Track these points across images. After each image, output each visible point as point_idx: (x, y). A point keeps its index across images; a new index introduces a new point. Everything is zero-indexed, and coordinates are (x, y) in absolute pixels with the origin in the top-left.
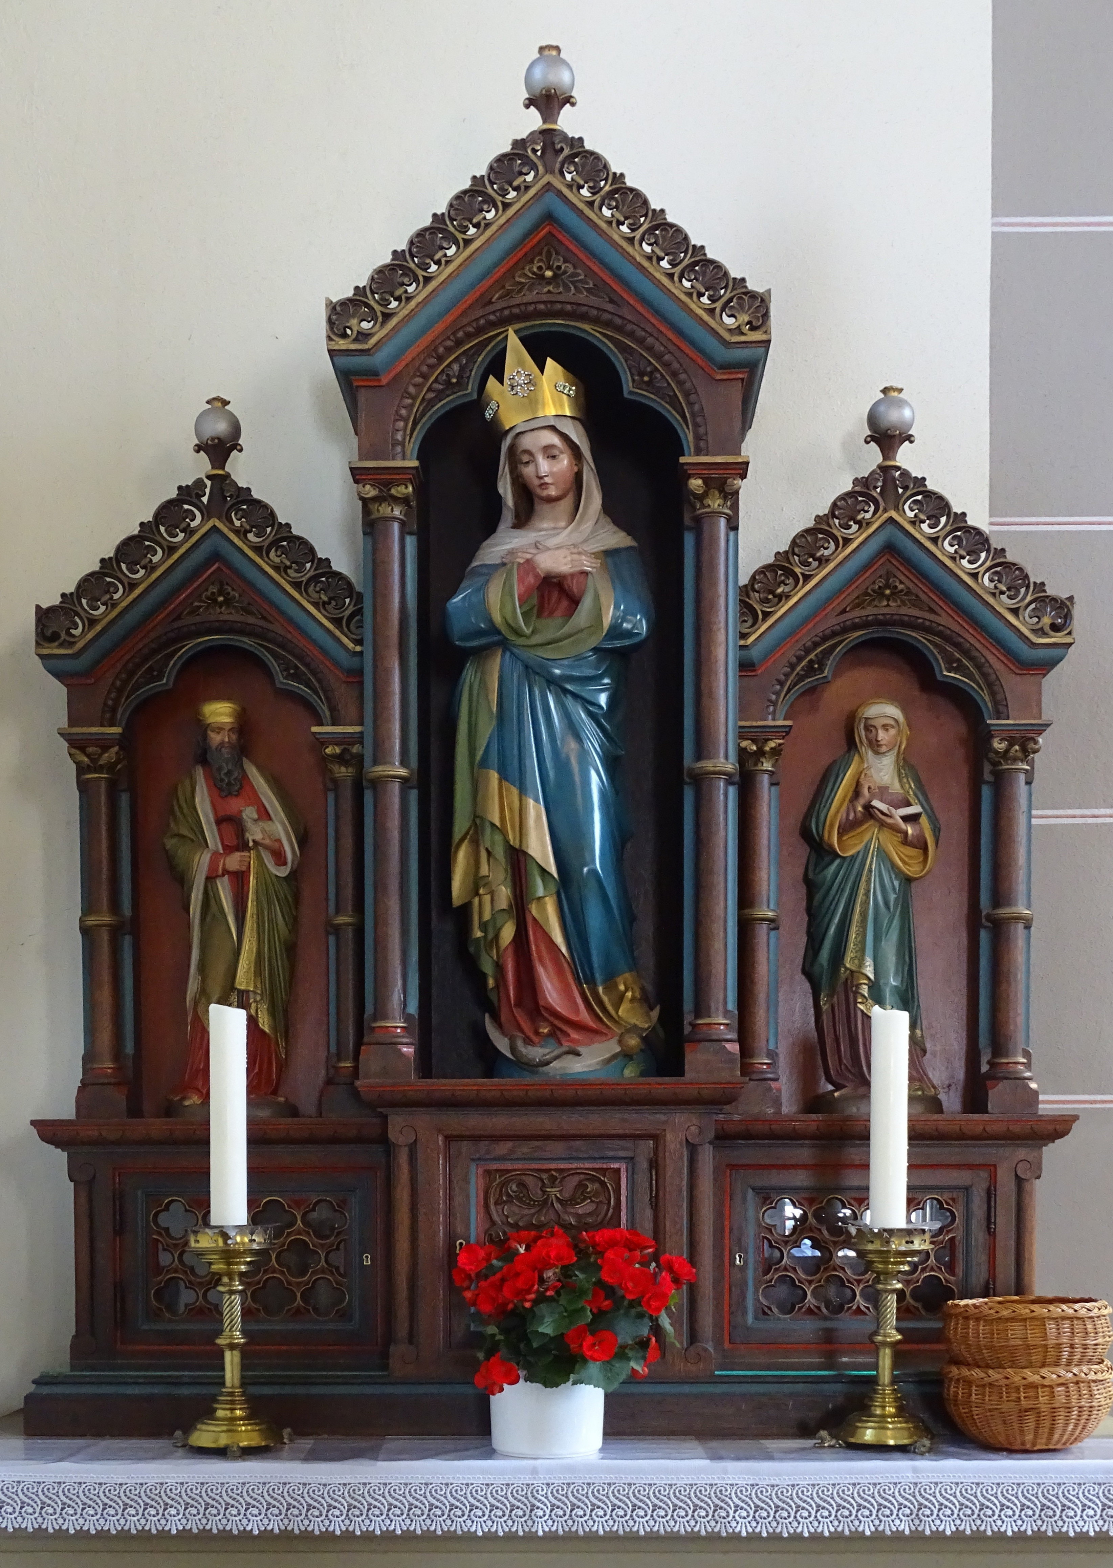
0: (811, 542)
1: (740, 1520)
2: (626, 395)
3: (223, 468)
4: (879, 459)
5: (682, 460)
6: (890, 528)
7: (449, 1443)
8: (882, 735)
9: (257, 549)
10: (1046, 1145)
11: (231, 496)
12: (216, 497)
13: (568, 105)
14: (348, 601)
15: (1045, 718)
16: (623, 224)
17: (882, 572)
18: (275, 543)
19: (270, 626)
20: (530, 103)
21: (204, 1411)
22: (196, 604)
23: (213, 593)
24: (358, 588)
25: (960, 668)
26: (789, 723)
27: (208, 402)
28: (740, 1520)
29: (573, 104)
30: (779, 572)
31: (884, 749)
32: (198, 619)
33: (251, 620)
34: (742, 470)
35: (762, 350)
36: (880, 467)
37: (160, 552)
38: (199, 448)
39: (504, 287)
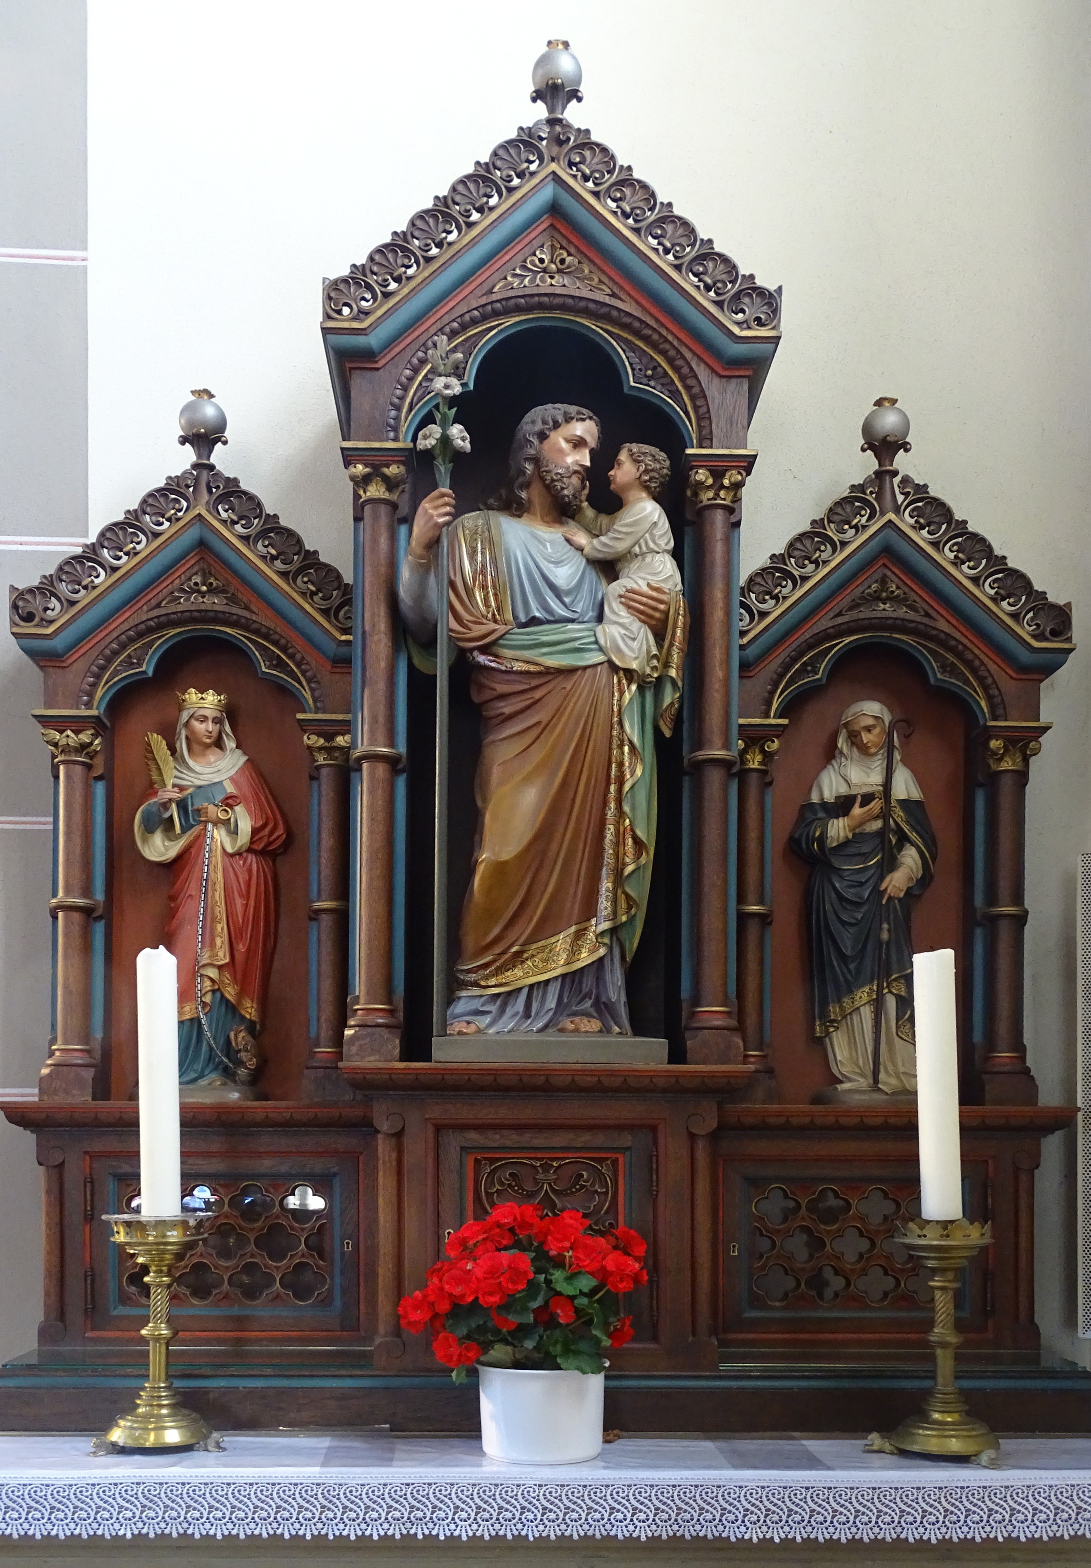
0: (810, 542)
1: (1040, 1525)
2: (626, 390)
3: (209, 459)
4: (874, 465)
5: (689, 451)
6: (888, 531)
7: (828, 1434)
8: (866, 737)
9: (245, 539)
10: (1045, 1136)
11: (218, 487)
12: (205, 484)
13: (575, 101)
14: (335, 593)
15: (1044, 719)
16: (237, 523)
17: (877, 576)
18: (263, 534)
19: (254, 618)
20: (538, 96)
21: (121, 1404)
22: (176, 594)
23: (196, 584)
24: (348, 578)
25: (952, 670)
26: (785, 721)
27: (193, 392)
28: (1040, 1525)
29: (580, 100)
30: (776, 572)
31: (873, 750)
32: (180, 608)
33: (235, 610)
34: (748, 464)
35: (771, 346)
36: (876, 473)
37: (102, 573)
38: (184, 440)
39: (505, 278)
